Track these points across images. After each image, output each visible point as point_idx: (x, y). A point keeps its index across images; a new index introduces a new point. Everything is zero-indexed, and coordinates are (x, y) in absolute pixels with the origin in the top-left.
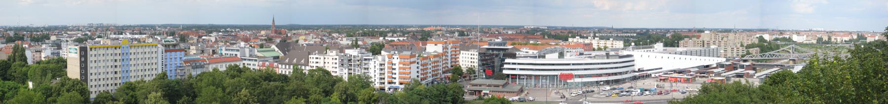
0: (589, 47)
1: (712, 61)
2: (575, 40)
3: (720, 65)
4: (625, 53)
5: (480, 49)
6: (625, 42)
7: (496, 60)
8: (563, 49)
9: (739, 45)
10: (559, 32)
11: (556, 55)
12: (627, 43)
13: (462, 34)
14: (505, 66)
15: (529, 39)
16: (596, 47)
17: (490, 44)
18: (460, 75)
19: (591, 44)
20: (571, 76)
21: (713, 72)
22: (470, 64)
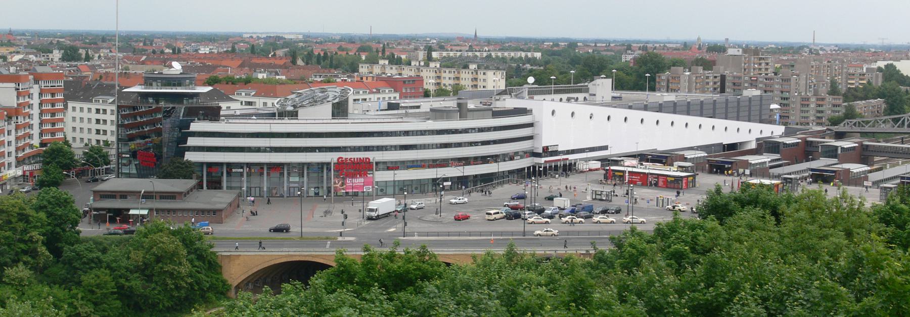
1: (747, 132)
2: (377, 70)
3: (766, 146)
4: (510, 103)
5: (122, 95)
8: (345, 92)
9: (823, 91)
10: (333, 48)
11: (326, 110)
13: (70, 54)
14: (192, 142)
15: (255, 67)
16: (432, 88)
20: (363, 168)
21: (746, 164)
22: (94, 137)
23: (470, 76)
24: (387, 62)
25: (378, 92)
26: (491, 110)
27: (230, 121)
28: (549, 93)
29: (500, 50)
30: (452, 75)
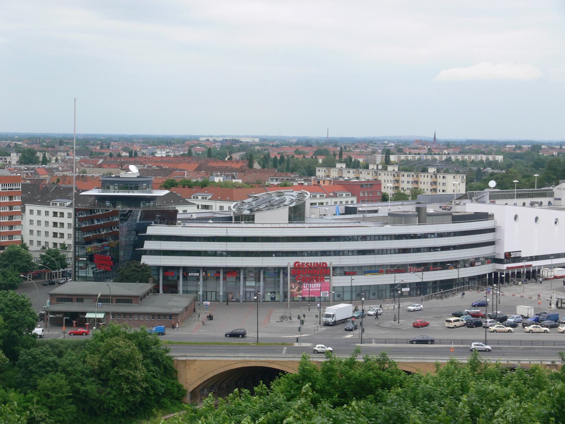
0: (372, 192)
2: (334, 173)
4: (471, 207)
5: (79, 199)
6: (469, 181)
7: (123, 229)
10: (290, 152)
11: (284, 213)
12: (476, 181)
13: (28, 158)
14: (148, 245)
15: (212, 171)
17: (105, 185)
18: (25, 270)
19: (376, 184)
22: (51, 240)
23: (429, 180)
24: (344, 166)
25: (335, 196)
26: (451, 214)
27: (187, 225)
28: (512, 197)
29: (460, 153)
30: (411, 179)
